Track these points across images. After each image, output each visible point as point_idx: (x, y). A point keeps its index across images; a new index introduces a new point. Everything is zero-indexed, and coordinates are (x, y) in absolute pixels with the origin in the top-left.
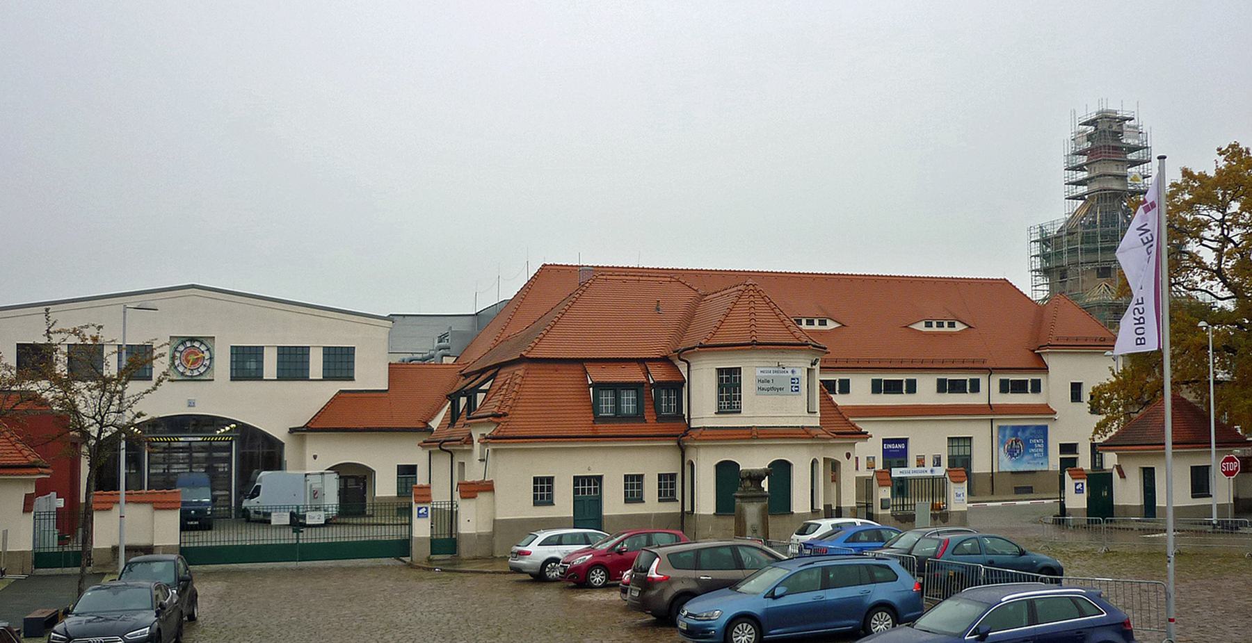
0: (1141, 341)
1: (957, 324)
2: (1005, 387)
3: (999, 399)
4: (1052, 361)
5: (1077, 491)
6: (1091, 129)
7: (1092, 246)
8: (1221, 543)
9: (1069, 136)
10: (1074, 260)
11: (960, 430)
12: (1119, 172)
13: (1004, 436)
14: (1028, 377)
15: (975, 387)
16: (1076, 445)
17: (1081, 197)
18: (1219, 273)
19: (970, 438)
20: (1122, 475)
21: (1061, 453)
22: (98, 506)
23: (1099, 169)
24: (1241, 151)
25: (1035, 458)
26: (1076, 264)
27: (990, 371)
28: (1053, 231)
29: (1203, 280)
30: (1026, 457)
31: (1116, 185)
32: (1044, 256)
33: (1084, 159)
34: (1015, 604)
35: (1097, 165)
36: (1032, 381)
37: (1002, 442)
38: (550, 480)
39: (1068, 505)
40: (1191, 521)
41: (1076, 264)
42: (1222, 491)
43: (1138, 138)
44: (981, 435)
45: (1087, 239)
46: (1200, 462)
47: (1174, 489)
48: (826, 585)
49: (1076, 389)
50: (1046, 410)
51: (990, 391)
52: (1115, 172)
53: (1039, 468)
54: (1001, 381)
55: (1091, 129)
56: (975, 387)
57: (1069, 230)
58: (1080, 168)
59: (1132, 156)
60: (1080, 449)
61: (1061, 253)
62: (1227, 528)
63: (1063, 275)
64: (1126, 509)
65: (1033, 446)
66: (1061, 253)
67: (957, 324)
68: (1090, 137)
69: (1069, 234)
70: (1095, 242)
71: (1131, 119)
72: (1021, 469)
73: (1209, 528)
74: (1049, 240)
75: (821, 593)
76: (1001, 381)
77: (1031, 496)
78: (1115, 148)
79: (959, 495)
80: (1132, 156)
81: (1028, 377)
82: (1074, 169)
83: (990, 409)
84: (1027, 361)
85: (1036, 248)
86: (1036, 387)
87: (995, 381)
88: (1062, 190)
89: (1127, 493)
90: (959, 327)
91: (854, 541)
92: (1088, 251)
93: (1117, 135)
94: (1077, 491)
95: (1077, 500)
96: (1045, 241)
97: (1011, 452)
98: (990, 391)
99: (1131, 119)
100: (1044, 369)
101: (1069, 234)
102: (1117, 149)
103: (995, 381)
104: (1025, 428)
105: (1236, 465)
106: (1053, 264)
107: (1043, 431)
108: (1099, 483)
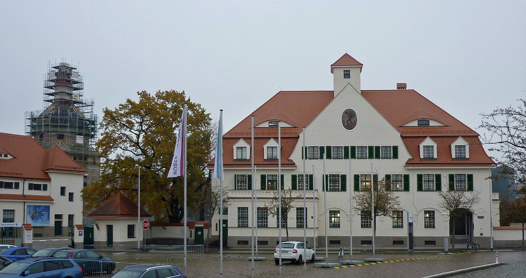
0: (175, 173)
1: (9, 156)
2: (31, 187)
3: (28, 192)
4: (53, 176)
5: (80, 235)
6: (57, 71)
7: (56, 124)
8: (139, 256)
9: (46, 71)
10: (47, 130)
11: (9, 206)
12: (69, 92)
13: (30, 210)
14: (42, 183)
15: (17, 186)
16: (62, 215)
17: (51, 101)
18: (137, 144)
19: (14, 210)
20: (98, 228)
21: (55, 218)
22: (316, 206)
23: (60, 89)
24: (147, 95)
25: (43, 221)
26: (48, 132)
27: (25, 179)
28: (37, 115)
29: (130, 146)
30: (40, 220)
31: (67, 98)
32: (32, 127)
33: (53, 84)
34: (150, 272)
35: (59, 87)
36: (15, 183)
37: (29, 213)
38: (56, 215)
39: (76, 241)
40: (130, 248)
41: (48, 132)
42: (139, 236)
43: (78, 78)
44: (19, 208)
45: (53, 120)
46: (131, 223)
47: (120, 235)
48: (45, 270)
49: (63, 189)
50: (49, 199)
51: (24, 189)
52: (67, 91)
53: (45, 226)
54: (29, 184)
55: (57, 71)
56: (17, 186)
57: (45, 115)
58: (51, 88)
59: (75, 86)
60: (64, 217)
61: (41, 126)
62: (143, 250)
63: (41, 136)
64: (99, 243)
65: (43, 215)
66: (41, 126)
67: (9, 156)
68: (56, 74)
69: (45, 117)
70: (57, 122)
71: (75, 69)
72: (37, 226)
73: (137, 250)
74: (35, 119)
75: (44, 273)
76: (29, 184)
77: (42, 238)
78: (68, 81)
79: (28, 236)
80: (75, 86)
81: (42, 183)
82: (48, 87)
83: (24, 197)
84: (41, 175)
85: (29, 122)
86: (45, 188)
87: (27, 184)
88: (43, 97)
89: (100, 236)
90: (9, 157)
91: (15, 254)
92: (54, 126)
93: (69, 75)
94: (80, 235)
95: (79, 239)
96: (33, 119)
97: (33, 218)
98: (24, 189)
99: (75, 69)
100: (49, 180)
101: (45, 117)
102: (69, 81)
103: (27, 184)
104: (39, 207)
105: (147, 225)
106: (37, 130)
107: (47, 209)
108: (88, 232)
